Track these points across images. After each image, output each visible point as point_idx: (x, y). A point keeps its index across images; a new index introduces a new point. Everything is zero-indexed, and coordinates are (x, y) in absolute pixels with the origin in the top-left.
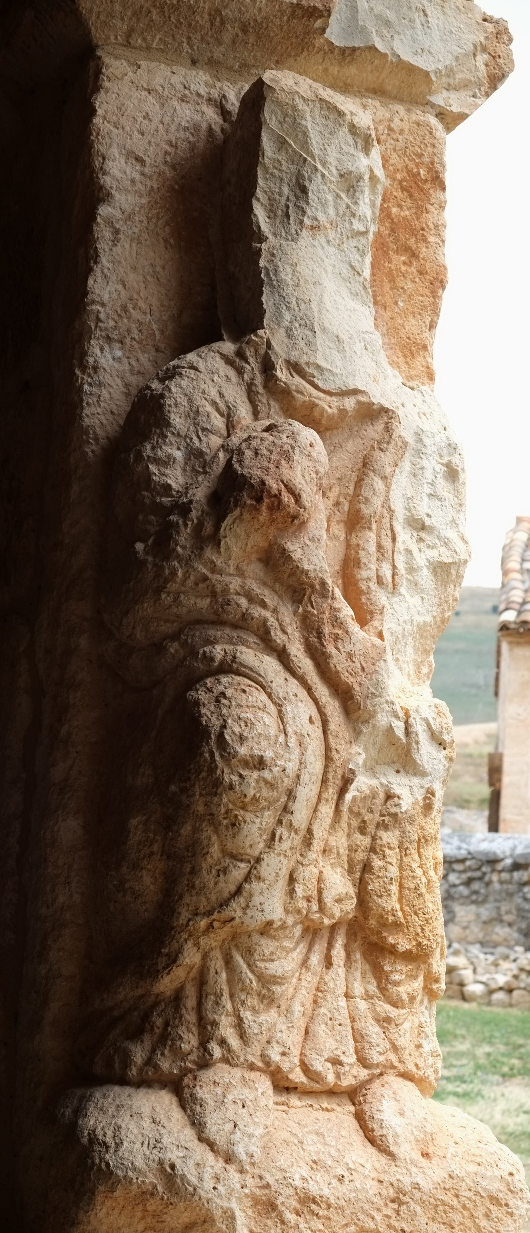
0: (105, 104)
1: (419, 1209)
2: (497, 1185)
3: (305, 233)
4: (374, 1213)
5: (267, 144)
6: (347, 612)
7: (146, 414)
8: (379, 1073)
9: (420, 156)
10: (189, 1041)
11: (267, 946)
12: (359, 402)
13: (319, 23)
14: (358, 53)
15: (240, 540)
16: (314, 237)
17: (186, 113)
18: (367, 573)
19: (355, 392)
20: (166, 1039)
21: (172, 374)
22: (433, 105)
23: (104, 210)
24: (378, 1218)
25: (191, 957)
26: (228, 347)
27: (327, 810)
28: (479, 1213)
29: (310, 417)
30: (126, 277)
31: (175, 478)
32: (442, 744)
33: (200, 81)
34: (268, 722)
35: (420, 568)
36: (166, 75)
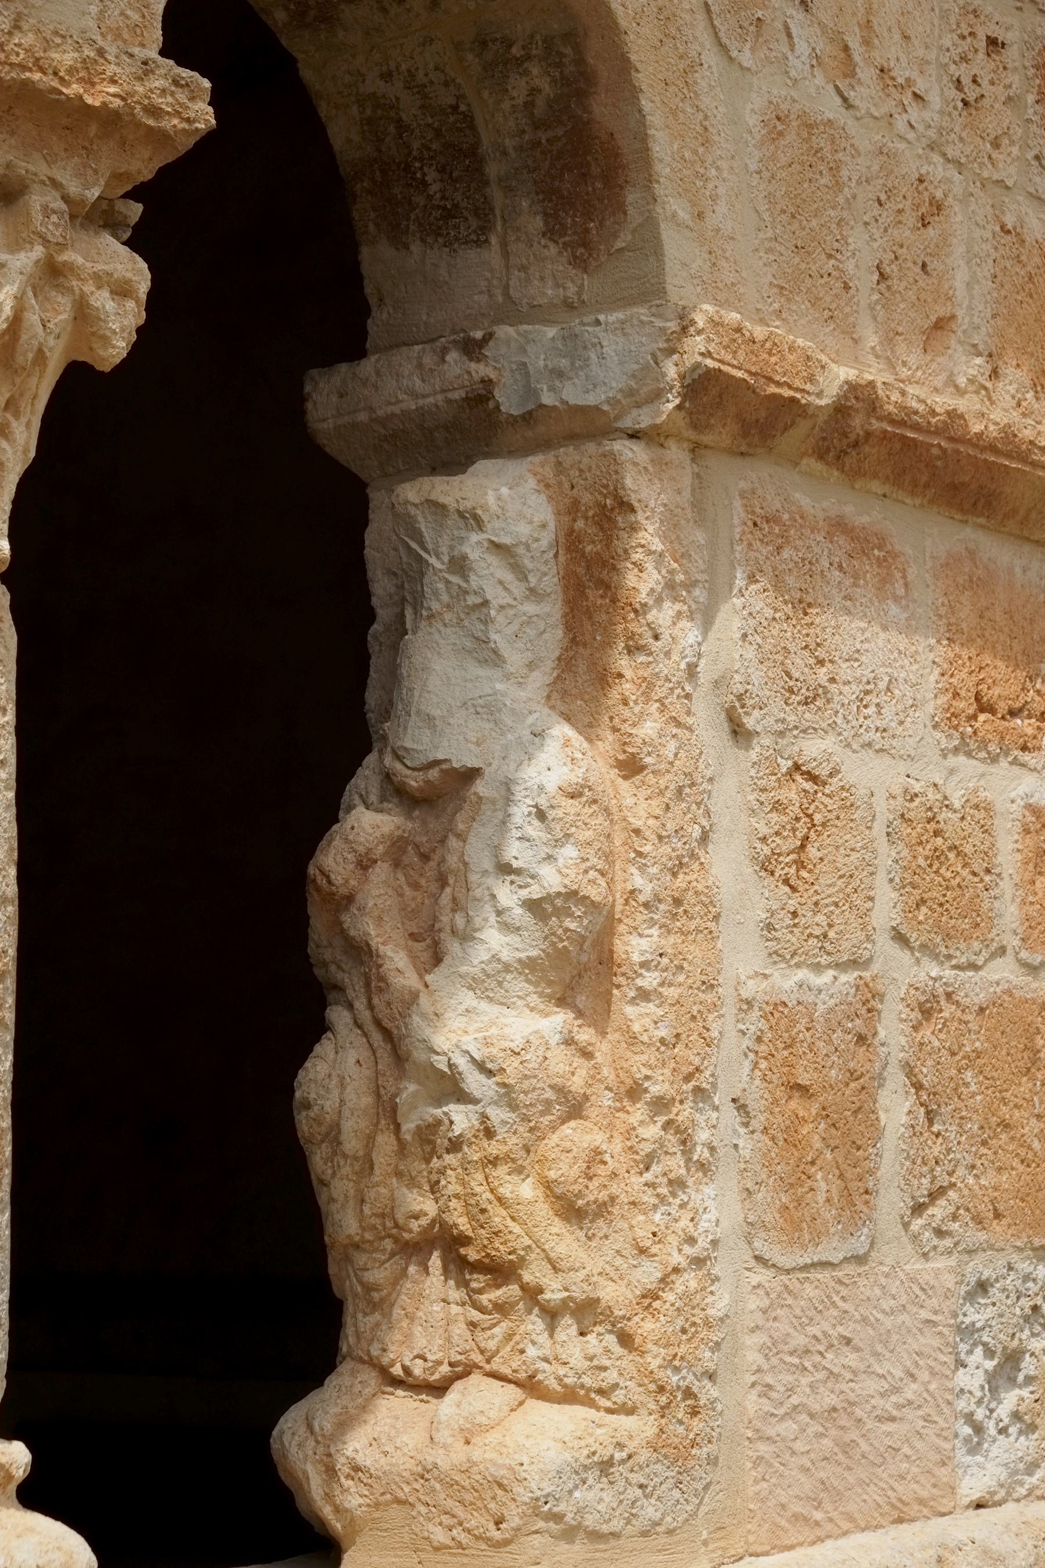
1: (438, 1486)
2: (503, 1472)
3: (423, 624)
4: (404, 1486)
9: (606, 486)
11: (361, 1259)
12: (442, 771)
13: (491, 404)
14: (534, 414)
16: (430, 625)
19: (437, 763)
22: (621, 430)
24: (407, 1489)
28: (488, 1496)
32: (490, 1073)
35: (509, 909)
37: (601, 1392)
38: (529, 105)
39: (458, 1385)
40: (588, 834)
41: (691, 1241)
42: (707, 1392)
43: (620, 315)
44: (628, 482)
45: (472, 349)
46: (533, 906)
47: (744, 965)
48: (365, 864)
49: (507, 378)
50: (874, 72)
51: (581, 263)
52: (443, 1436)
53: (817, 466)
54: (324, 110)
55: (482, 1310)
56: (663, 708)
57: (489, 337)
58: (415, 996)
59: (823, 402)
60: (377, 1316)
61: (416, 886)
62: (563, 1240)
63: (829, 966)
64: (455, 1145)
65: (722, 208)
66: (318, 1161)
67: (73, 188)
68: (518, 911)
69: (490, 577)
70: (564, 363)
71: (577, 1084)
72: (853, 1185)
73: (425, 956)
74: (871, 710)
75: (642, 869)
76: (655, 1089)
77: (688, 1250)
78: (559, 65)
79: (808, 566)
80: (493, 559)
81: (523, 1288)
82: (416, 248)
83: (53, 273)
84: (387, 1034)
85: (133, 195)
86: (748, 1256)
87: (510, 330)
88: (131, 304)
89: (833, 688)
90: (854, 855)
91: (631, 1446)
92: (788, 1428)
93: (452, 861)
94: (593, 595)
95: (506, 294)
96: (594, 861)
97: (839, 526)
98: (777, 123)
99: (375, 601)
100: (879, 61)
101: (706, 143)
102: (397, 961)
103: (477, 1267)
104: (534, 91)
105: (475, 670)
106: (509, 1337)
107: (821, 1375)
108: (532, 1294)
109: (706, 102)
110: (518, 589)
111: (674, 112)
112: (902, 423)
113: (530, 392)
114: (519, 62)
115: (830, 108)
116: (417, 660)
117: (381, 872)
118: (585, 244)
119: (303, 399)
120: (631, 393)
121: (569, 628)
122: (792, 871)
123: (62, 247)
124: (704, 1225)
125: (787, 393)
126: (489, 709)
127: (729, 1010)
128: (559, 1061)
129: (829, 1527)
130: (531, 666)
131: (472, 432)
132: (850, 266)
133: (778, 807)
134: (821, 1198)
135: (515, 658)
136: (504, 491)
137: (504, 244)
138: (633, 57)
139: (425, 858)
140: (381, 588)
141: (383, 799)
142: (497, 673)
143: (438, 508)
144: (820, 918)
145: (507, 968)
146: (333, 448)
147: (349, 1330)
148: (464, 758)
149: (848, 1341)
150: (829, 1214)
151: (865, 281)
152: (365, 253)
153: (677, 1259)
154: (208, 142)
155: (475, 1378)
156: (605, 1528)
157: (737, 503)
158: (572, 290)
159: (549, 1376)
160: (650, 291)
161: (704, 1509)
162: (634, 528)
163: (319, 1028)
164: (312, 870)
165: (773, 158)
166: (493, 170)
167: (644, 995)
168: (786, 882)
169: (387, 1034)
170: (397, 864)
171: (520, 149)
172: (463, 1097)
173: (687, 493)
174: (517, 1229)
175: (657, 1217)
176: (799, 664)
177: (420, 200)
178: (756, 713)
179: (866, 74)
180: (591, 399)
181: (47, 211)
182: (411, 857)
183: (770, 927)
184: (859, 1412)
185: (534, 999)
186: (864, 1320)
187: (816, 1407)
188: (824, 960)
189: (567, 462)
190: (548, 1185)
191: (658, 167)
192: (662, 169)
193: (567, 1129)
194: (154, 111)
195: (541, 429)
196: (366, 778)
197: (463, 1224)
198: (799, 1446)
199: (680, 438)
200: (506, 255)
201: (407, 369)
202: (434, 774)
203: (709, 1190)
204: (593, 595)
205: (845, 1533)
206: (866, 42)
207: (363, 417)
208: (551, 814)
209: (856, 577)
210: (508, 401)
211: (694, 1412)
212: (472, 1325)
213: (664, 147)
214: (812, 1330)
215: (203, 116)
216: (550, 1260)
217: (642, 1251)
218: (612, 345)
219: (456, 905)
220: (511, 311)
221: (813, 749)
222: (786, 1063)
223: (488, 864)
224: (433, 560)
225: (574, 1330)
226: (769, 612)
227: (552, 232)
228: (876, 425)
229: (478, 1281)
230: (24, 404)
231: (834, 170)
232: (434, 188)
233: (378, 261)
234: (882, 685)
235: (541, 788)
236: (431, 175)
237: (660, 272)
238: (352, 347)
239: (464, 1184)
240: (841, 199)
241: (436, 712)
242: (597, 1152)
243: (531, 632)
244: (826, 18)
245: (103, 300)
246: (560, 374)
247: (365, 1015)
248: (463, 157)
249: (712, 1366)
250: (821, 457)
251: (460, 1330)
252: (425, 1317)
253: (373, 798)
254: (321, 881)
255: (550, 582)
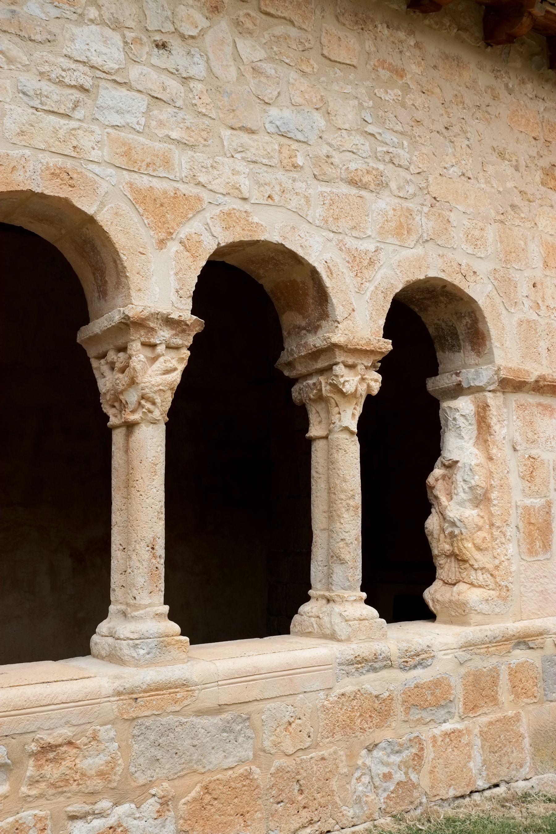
11: (439, 559)
37: (487, 586)
38: (466, 325)
39: (457, 584)
40: (481, 473)
41: (506, 555)
42: (511, 586)
43: (486, 367)
44: (488, 401)
45: (457, 374)
46: (470, 488)
47: (517, 497)
48: (437, 480)
49: (464, 380)
50: (545, 307)
51: (478, 356)
52: (454, 594)
53: (533, 393)
54: (427, 326)
55: (462, 569)
56: (497, 447)
57: (460, 372)
58: (447, 507)
59: (532, 380)
60: (442, 570)
61: (448, 484)
62: (478, 555)
63: (539, 498)
65: (508, 342)
66: (429, 538)
67: (366, 364)
68: (467, 489)
69: (461, 421)
70: (475, 377)
71: (480, 524)
72: (546, 544)
73: (450, 498)
74: (549, 443)
75: (493, 480)
76: (497, 525)
77: (506, 557)
78: (471, 317)
79: (532, 414)
80: (461, 418)
81: (470, 565)
83: (363, 379)
84: (442, 514)
85: (379, 362)
86: (520, 558)
87: (464, 370)
88: (378, 383)
89: (539, 439)
90: (544, 474)
91: (493, 597)
92: (531, 594)
93: (454, 479)
96: (482, 479)
97: (540, 404)
98: (521, 323)
99: (442, 425)
100: (546, 304)
101: (504, 329)
102: (443, 499)
103: (460, 560)
104: (467, 322)
105: (459, 440)
106: (467, 575)
107: (539, 583)
108: (472, 566)
109: (503, 321)
110: (467, 423)
111: (496, 325)
112: (553, 382)
113: (469, 383)
114: (464, 317)
115: (534, 317)
116: (447, 439)
117: (440, 481)
118: (479, 352)
119: (426, 384)
120: (488, 383)
121: (478, 431)
122: (529, 478)
123: (364, 375)
124: (509, 552)
125: (523, 380)
126: (461, 448)
127: (514, 508)
128: (477, 520)
129: (542, 615)
130: (470, 439)
131: (458, 391)
132: (540, 349)
133: (525, 465)
134: (538, 546)
135: (466, 438)
136: (464, 404)
137: (464, 352)
138: (485, 316)
139: (449, 478)
140: (443, 422)
141: (441, 467)
142: (463, 441)
143: (450, 408)
144: (537, 488)
145: (465, 501)
146: (432, 394)
147: (437, 573)
148: (456, 458)
149: (546, 577)
150: (540, 550)
151: (544, 353)
153: (503, 559)
154: (391, 352)
155: (461, 583)
156: (487, 613)
157: (514, 403)
158: (477, 361)
159: (475, 582)
160: (492, 362)
161: (511, 610)
162: (490, 410)
163: (430, 513)
164: (427, 482)
165: (520, 330)
166: (461, 337)
167: (495, 505)
168: (527, 480)
169: (442, 514)
170: (444, 480)
171: (465, 333)
172: (457, 526)
173: (502, 402)
174: (468, 553)
175: (499, 551)
176: (530, 435)
177: (447, 343)
178: (519, 446)
179: (543, 308)
180: (481, 384)
181: (361, 369)
182: (447, 478)
183: (524, 490)
184: (549, 592)
185: (471, 507)
186: (550, 572)
187: (537, 590)
188: (537, 496)
189: (477, 397)
190: (474, 544)
191: (492, 337)
192: (493, 337)
193: (479, 533)
194: (381, 348)
195: (472, 390)
196: (438, 463)
197: (457, 552)
198: (533, 598)
199: (499, 391)
200: (464, 354)
201: (445, 378)
202: (450, 462)
203: (511, 545)
205: (546, 617)
206: (543, 301)
207: (437, 388)
208: (473, 470)
209: (544, 415)
210: (465, 385)
211: (508, 590)
212: (460, 572)
213: (493, 332)
214: (536, 574)
215: (390, 347)
216: (475, 560)
217: (495, 557)
218: (484, 373)
219: (455, 488)
220: (465, 366)
221: (534, 452)
222: (528, 518)
223: (461, 480)
224: (450, 418)
225: (480, 574)
226: (522, 425)
227: (473, 350)
228: (546, 383)
229: (461, 563)
230: (359, 404)
231: (535, 330)
232: (450, 341)
233: (440, 355)
234: (551, 437)
235: (471, 465)
237: (494, 358)
238: (435, 373)
239: (457, 544)
240: (537, 336)
241: (450, 449)
242: (485, 537)
243: (470, 432)
244: (533, 299)
245: (372, 384)
246: (474, 379)
247: (438, 510)
248: (455, 335)
249: (512, 581)
250: (534, 391)
251: (458, 573)
252: (446, 569)
253: (440, 466)
254: (428, 484)
255: (474, 422)
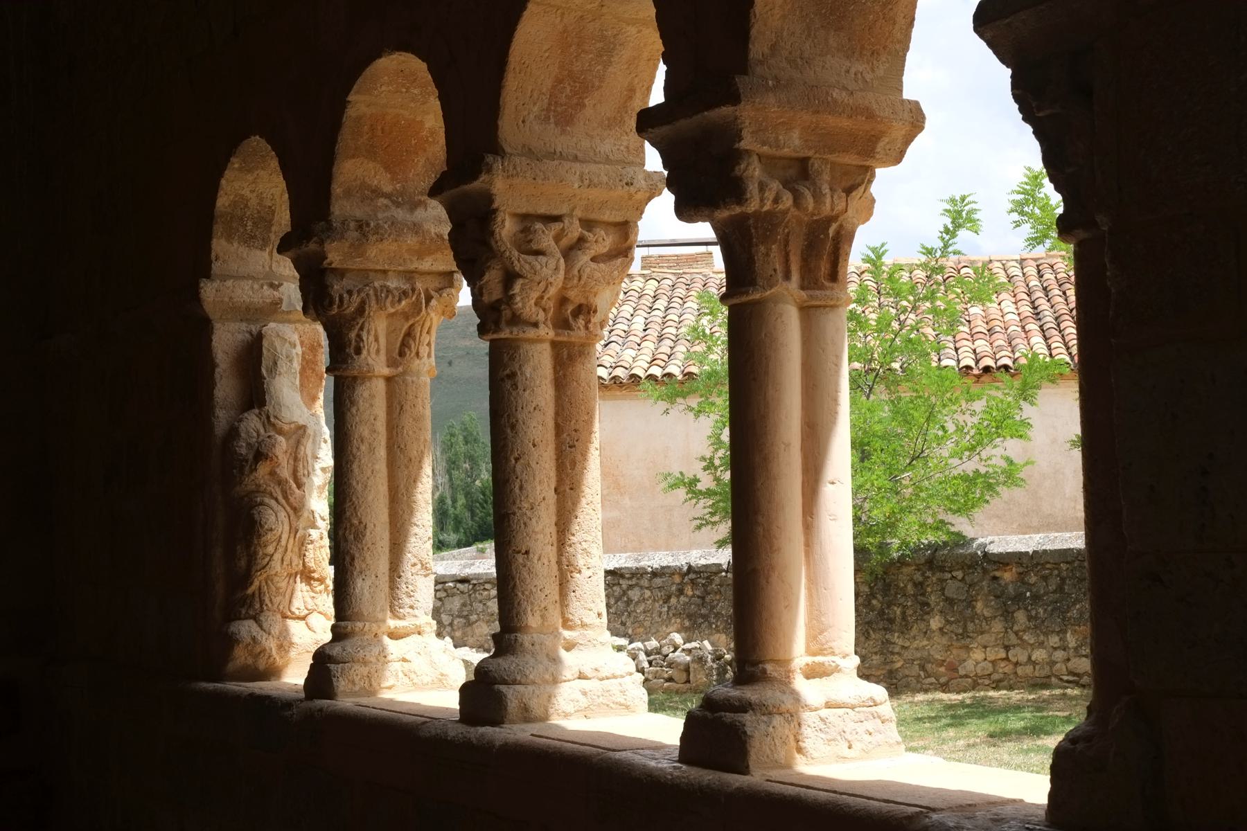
0: (215, 338)
5: (264, 351)
6: (294, 486)
7: (233, 433)
8: (311, 612)
10: (257, 606)
15: (263, 469)
17: (240, 337)
18: (300, 474)
20: (251, 605)
21: (241, 420)
23: (217, 370)
25: (256, 583)
26: (257, 411)
27: (291, 540)
29: (280, 432)
30: (225, 388)
31: (243, 451)
33: (244, 326)
34: (273, 518)
36: (234, 326)
57: (281, 285)
64: (312, 542)
82: (236, 244)
94: (309, 372)
95: (271, 267)
152: (214, 242)
204: (309, 372)
229: (315, 584)
236: (250, 223)
